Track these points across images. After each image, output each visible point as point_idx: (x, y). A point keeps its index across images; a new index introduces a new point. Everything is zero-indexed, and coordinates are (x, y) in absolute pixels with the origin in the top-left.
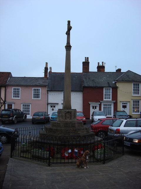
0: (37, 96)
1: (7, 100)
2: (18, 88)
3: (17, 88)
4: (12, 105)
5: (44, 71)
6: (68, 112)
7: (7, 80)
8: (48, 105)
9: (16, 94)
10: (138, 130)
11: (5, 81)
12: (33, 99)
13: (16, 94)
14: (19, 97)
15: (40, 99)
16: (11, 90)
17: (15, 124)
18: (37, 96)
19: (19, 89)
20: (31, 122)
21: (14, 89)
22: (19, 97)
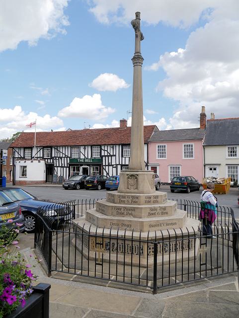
0: (189, 154)
1: (149, 161)
2: (190, 144)
3: (162, 145)
4: (156, 167)
5: (199, 119)
6: (132, 175)
7: (150, 136)
8: (205, 166)
9: (162, 153)
10: (197, 193)
11: (147, 137)
12: (184, 158)
13: (162, 153)
14: (165, 157)
15: (166, 159)
16: (154, 148)
17: (77, 189)
18: (189, 154)
19: (165, 146)
20: (169, 187)
21: (185, 145)
22: (165, 157)
